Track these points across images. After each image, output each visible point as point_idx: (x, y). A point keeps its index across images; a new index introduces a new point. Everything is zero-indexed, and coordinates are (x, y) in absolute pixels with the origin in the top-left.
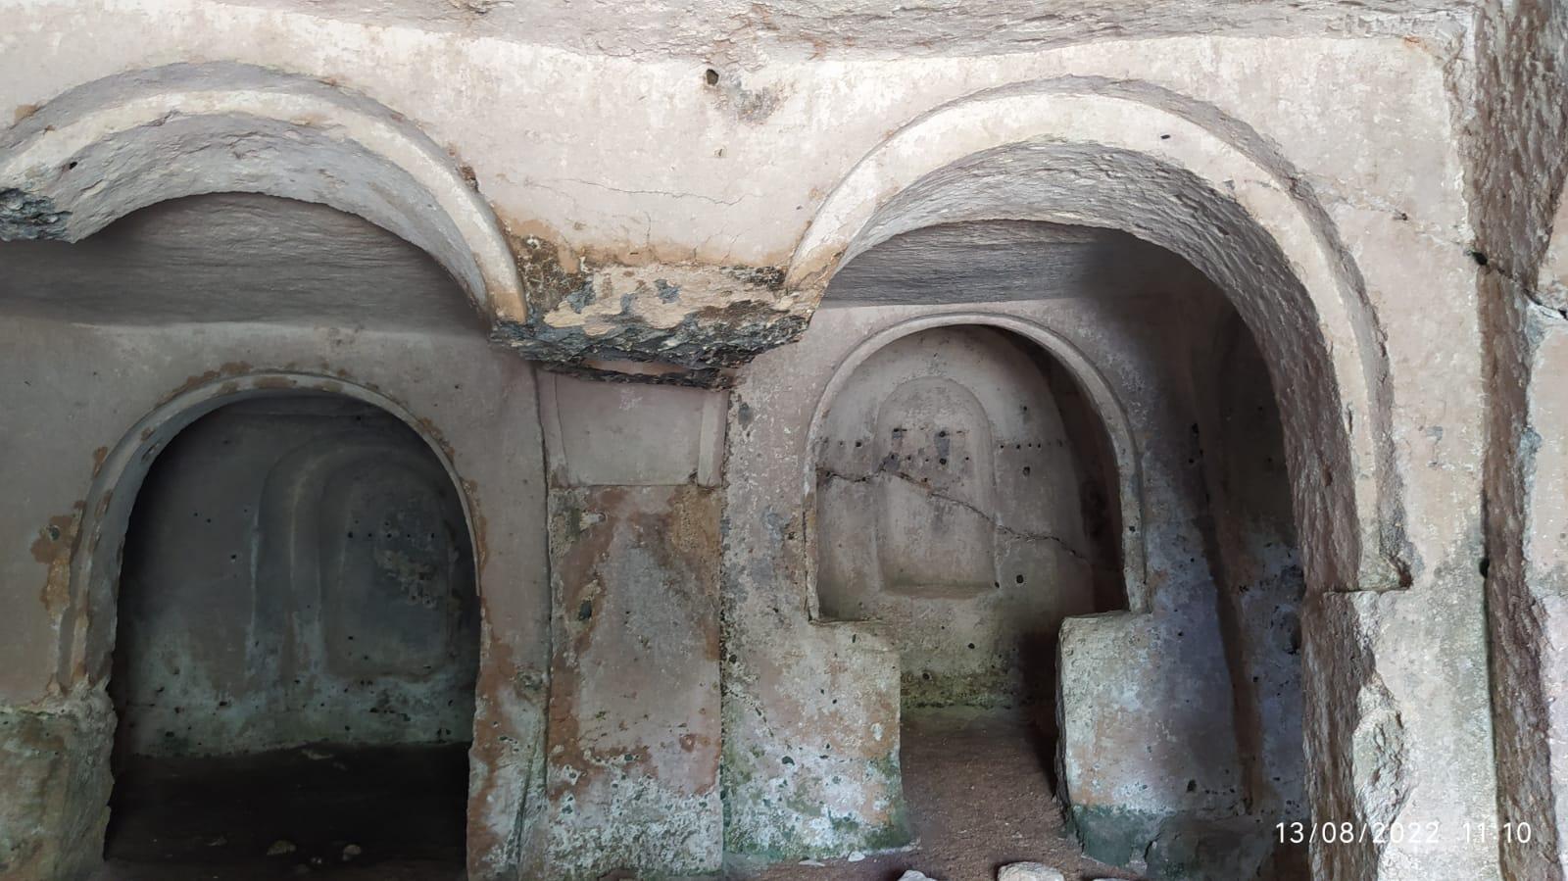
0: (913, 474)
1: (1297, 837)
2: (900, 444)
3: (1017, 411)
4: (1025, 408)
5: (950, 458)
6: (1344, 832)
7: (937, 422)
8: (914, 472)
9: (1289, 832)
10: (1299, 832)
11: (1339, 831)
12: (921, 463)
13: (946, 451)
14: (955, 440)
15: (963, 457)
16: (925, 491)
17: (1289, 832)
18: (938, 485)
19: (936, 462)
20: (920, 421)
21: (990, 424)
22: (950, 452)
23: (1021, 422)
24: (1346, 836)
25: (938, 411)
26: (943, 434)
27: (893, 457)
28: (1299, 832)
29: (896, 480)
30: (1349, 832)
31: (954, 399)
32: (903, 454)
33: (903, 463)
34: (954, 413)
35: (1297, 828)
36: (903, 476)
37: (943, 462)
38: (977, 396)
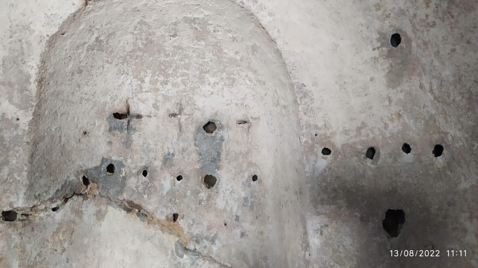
0: (150, 205)
1: (396, 255)
2: (128, 143)
3: (369, 53)
4: (396, 39)
5: (223, 176)
6: (411, 253)
7: (200, 102)
8: (154, 199)
9: (394, 253)
10: (397, 253)
11: (409, 253)
12: (166, 182)
13: (216, 160)
14: (231, 137)
15: (247, 175)
16: (170, 240)
17: (394, 253)
18: (196, 231)
19: (194, 182)
20: (166, 98)
21: (299, 93)
22: (224, 163)
23: (381, 76)
24: (412, 254)
25: (202, 80)
26: (209, 127)
27: (111, 168)
28: (397, 253)
29: (115, 215)
30: (412, 253)
31: (229, 51)
32: (132, 163)
33: (132, 182)
34: (232, 82)
35: (396, 252)
36: (131, 207)
37: (210, 181)
38: (265, 20)
